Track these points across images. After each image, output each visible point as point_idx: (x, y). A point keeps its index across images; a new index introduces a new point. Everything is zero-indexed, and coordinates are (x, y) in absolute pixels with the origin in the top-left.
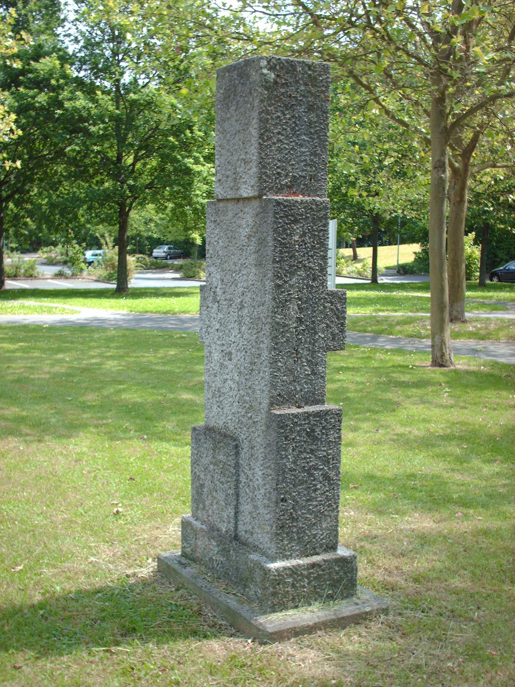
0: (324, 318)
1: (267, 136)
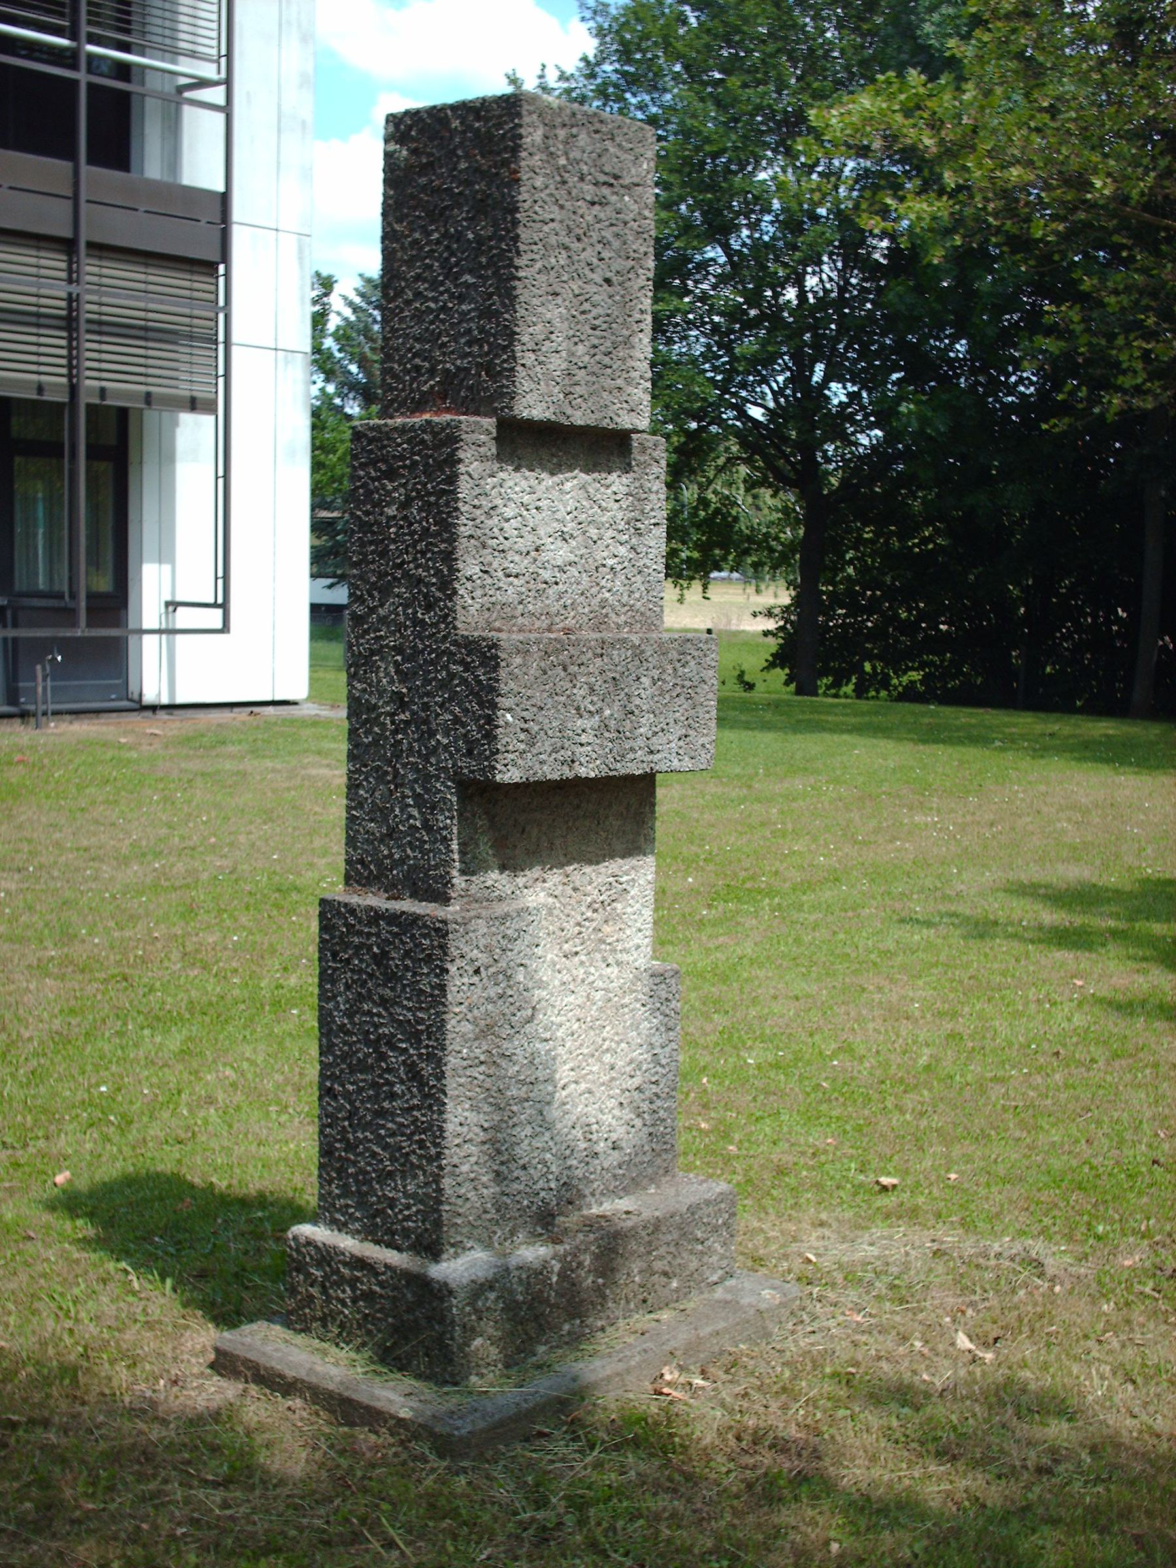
0: (451, 699)
1: (395, 289)
